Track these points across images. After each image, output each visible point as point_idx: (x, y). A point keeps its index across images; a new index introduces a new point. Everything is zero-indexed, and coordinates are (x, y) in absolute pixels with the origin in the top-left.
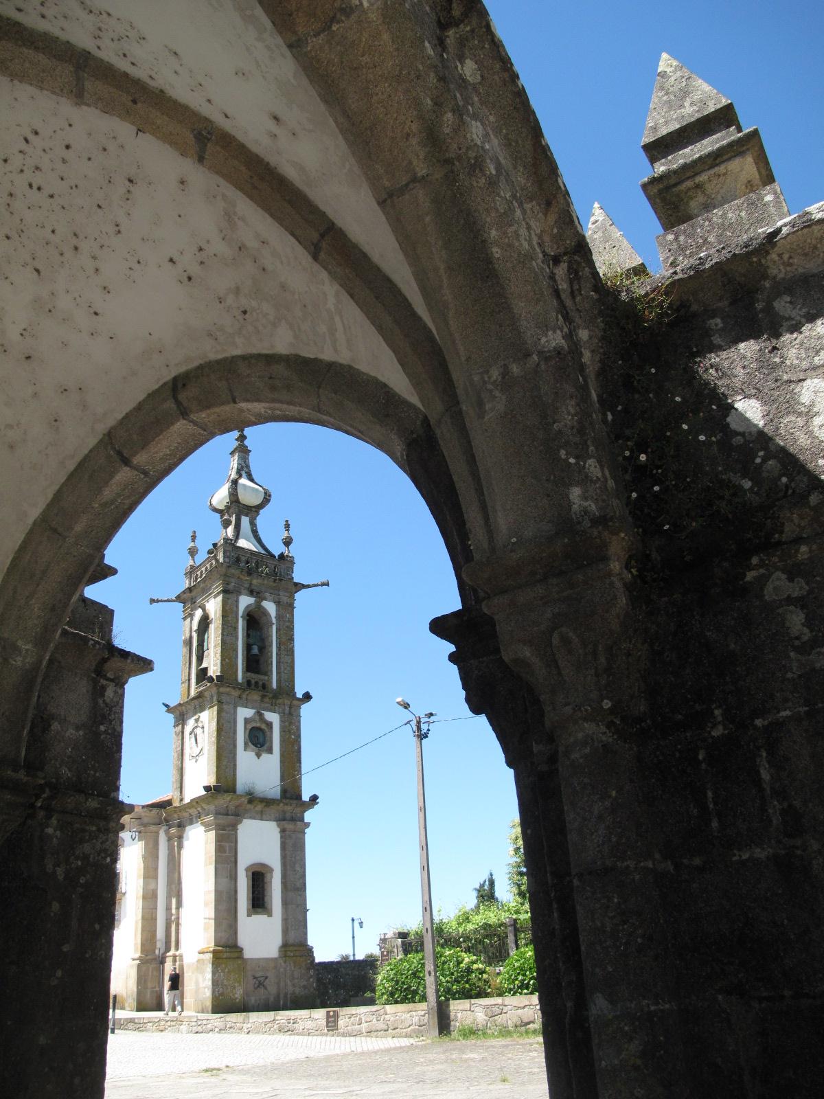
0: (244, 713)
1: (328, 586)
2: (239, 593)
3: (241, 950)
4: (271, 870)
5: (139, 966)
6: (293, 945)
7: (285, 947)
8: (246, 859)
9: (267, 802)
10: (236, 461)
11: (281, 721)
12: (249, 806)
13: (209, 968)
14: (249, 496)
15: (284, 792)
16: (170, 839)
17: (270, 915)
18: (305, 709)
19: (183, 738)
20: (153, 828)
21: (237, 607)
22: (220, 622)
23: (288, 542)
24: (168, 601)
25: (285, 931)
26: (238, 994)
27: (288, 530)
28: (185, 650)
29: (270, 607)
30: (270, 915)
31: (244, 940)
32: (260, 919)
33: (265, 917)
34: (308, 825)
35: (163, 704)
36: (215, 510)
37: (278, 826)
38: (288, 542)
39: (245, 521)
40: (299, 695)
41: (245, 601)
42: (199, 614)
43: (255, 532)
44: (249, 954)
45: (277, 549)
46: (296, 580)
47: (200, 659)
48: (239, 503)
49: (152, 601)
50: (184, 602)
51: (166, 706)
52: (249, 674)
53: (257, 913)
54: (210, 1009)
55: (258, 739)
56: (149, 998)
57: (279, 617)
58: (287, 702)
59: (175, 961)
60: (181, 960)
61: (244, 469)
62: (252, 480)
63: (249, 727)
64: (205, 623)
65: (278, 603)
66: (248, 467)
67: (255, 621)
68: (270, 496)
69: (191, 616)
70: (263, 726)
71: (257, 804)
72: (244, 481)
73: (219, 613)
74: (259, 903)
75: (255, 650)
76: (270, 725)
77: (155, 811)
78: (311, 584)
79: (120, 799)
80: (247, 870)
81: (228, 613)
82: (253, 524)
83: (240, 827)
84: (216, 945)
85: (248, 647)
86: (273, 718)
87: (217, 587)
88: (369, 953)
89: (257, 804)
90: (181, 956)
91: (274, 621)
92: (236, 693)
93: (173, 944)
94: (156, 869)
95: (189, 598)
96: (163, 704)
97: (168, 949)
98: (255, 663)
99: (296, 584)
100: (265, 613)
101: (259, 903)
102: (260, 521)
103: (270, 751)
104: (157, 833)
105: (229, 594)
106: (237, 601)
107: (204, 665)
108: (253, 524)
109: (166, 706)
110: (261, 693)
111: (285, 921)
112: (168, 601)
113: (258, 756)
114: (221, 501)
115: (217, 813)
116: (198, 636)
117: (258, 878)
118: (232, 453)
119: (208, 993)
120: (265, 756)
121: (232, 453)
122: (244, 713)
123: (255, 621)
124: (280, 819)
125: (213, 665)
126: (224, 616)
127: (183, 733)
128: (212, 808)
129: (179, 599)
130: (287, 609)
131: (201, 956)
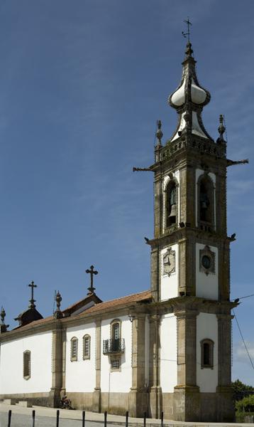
0: (200, 247)
1: (248, 162)
2: (196, 167)
3: (198, 388)
4: (213, 342)
5: (137, 393)
6: (224, 386)
7: (220, 386)
8: (200, 336)
9: (212, 302)
10: (187, 69)
11: (219, 253)
12: (203, 305)
13: (183, 397)
14: (198, 97)
15: (220, 296)
16: (150, 322)
17: (212, 367)
18: (232, 245)
19: (158, 261)
20: (143, 315)
21: (195, 177)
22: (184, 187)
23: (222, 131)
24: (145, 170)
25: (220, 379)
26: (198, 412)
27: (159, 128)
28: (157, 204)
29: (213, 176)
30: (212, 367)
31: (199, 383)
32: (207, 370)
33: (210, 369)
34: (233, 317)
35: (145, 238)
36: (173, 106)
37: (217, 316)
38: (222, 131)
39: (194, 114)
40: (229, 235)
41: (199, 172)
42: (167, 179)
43: (200, 123)
44: (202, 390)
45: (215, 136)
46: (228, 158)
47: (169, 210)
48: (179, 107)
49: (135, 169)
50: (155, 171)
51: (147, 240)
52: (202, 222)
53: (206, 367)
54: (184, 418)
55: (207, 263)
56: (143, 411)
57: (218, 183)
58: (223, 240)
59: (157, 392)
60: (161, 391)
61: (193, 78)
62: (198, 85)
63: (202, 255)
64: (172, 185)
65: (216, 174)
66: (195, 74)
67: (204, 184)
68: (210, 97)
69: (161, 180)
70: (210, 255)
71: (207, 304)
72: (193, 86)
73: (184, 181)
74: (207, 362)
75: (205, 206)
76: (213, 254)
77: (143, 305)
78: (237, 161)
79: (201, 313)
80: (202, 342)
81: (190, 179)
82: (199, 117)
83: (198, 317)
84: (187, 384)
85: (201, 203)
86: (214, 249)
87: (183, 163)
88: (201, 387)
89: (207, 304)
90: (161, 389)
91: (215, 187)
92: (195, 234)
93: (155, 383)
94: (144, 339)
95: (159, 169)
96: (145, 238)
97: (151, 384)
98: (204, 214)
99: (228, 161)
100: (210, 181)
101: (207, 362)
102: (203, 115)
103: (213, 270)
104: (145, 318)
105: (190, 168)
106: (195, 173)
107: (171, 215)
108: (199, 117)
109: (147, 240)
110: (209, 234)
111: (220, 372)
112: (145, 170)
113: (207, 274)
114: (179, 101)
115: (187, 309)
116: (167, 195)
117: (207, 346)
118: (184, 64)
119: (183, 410)
120: (211, 275)
121: (184, 64)
122: (200, 247)
123: (204, 184)
124: (218, 313)
125: (180, 213)
126: (188, 183)
127: (158, 257)
128: (184, 305)
129: (151, 169)
130: (222, 177)
131: (177, 390)
